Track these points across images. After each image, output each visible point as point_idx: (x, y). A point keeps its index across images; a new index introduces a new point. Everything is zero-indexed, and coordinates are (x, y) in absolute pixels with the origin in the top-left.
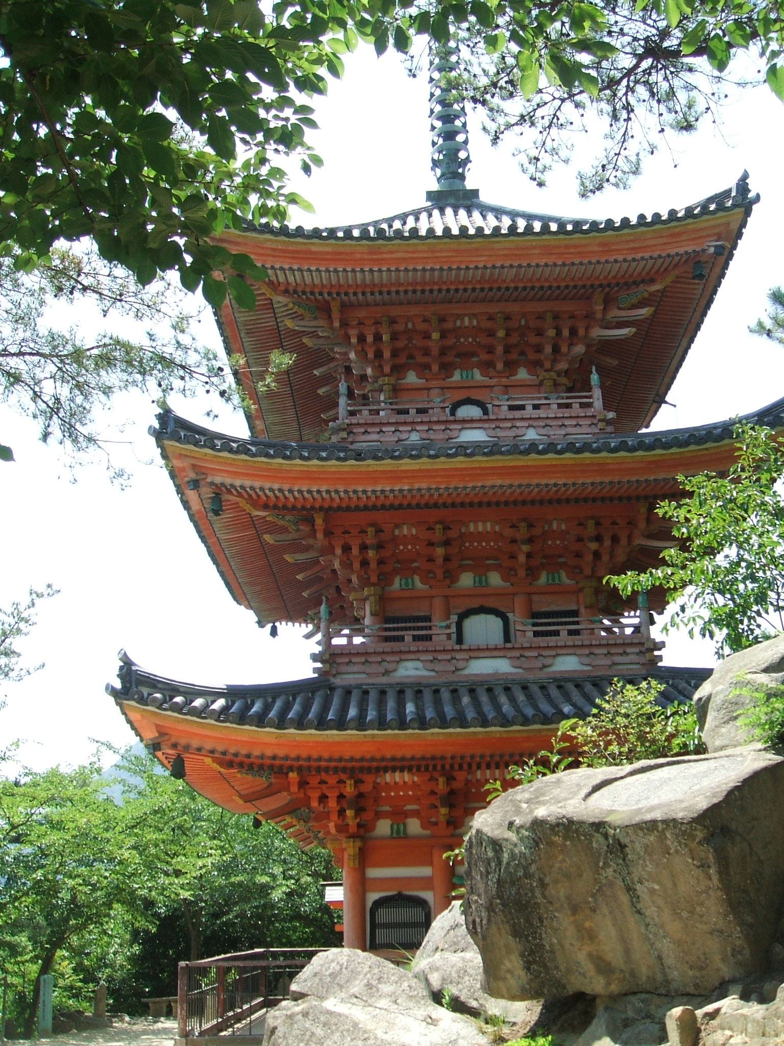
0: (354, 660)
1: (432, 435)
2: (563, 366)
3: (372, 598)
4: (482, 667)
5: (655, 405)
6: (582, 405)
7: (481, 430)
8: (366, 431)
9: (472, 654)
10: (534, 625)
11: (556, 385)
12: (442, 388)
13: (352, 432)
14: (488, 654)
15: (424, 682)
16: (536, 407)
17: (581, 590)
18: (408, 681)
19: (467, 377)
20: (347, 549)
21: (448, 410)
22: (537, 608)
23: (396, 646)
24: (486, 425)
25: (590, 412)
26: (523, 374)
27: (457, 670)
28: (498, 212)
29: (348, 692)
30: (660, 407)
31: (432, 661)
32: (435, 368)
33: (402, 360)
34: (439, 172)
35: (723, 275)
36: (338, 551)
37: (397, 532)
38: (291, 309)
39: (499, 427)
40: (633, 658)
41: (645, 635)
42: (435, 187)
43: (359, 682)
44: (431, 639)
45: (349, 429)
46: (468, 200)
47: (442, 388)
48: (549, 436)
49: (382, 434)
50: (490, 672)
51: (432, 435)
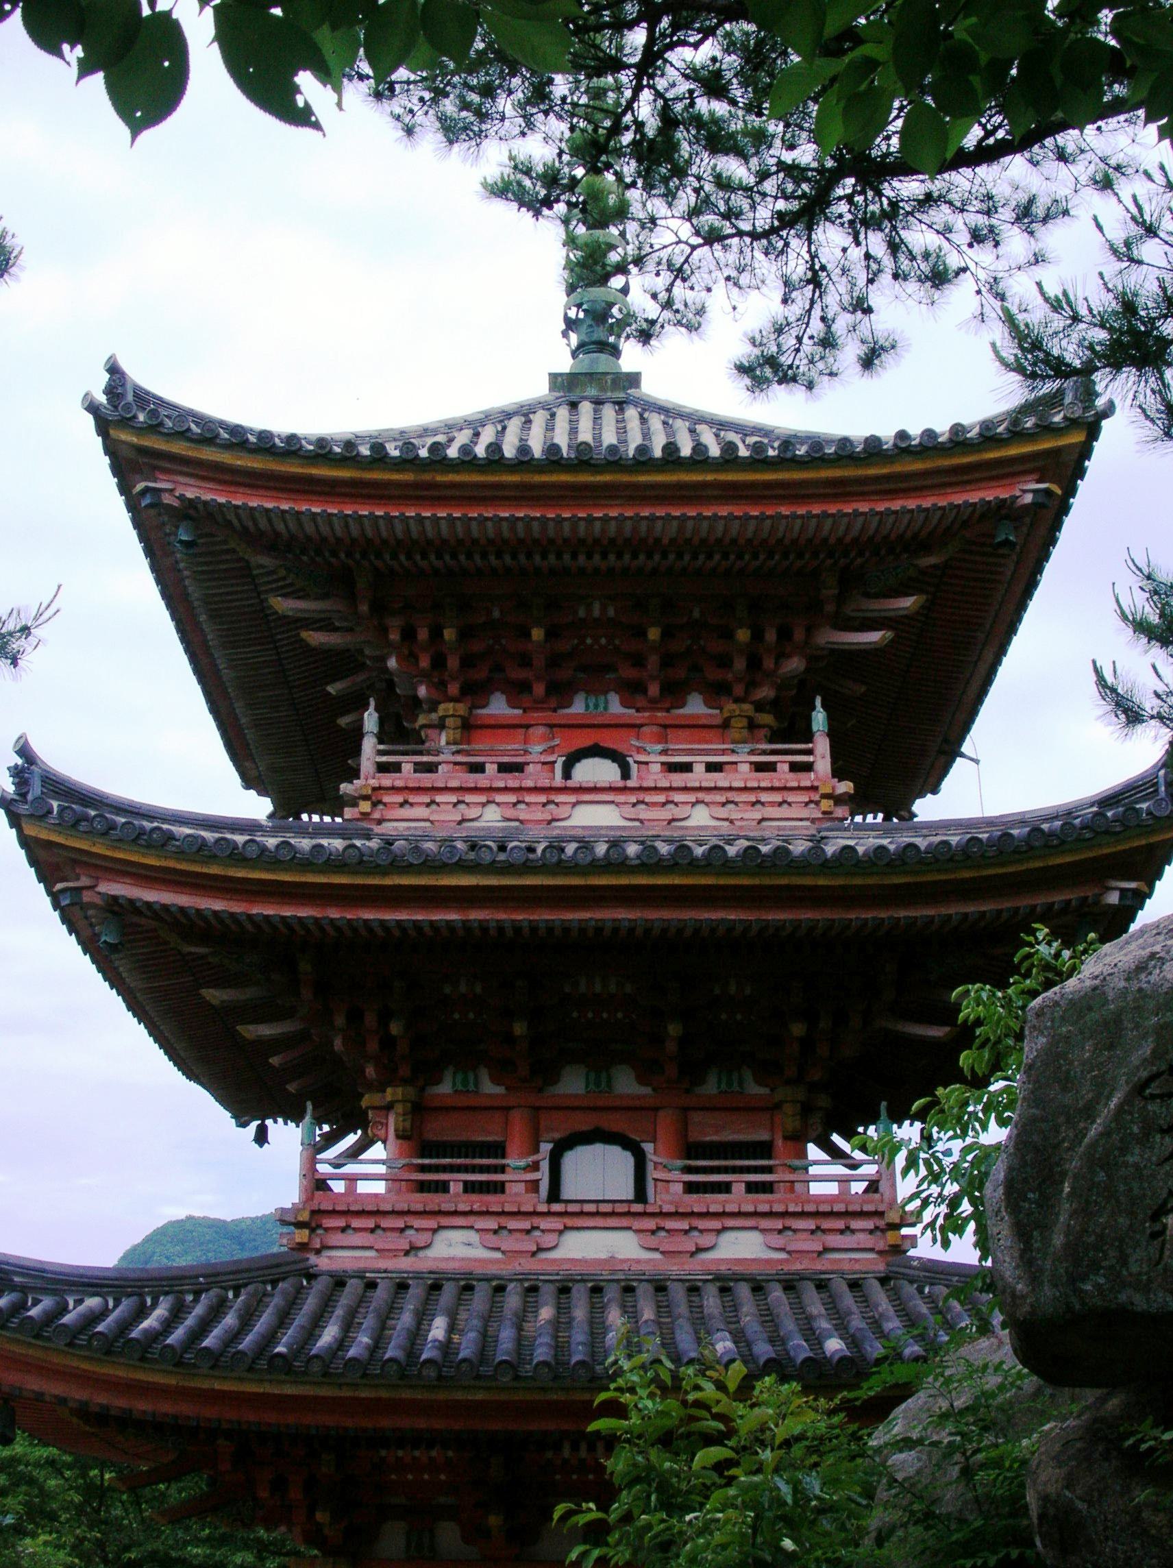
0: (356, 1223)
1: (522, 812)
2: (765, 692)
3: (399, 1108)
4: (586, 1247)
5: (943, 759)
6: (795, 767)
7: (613, 807)
8: (406, 802)
9: (570, 1222)
10: (689, 1170)
11: (752, 726)
12: (551, 726)
13: (380, 802)
14: (599, 1222)
15: (479, 1271)
16: (712, 767)
17: (777, 1107)
18: (451, 1266)
19: (596, 706)
20: (355, 1016)
21: (558, 768)
22: (695, 1136)
23: (434, 1201)
24: (620, 798)
25: (806, 779)
26: (695, 707)
27: (540, 1250)
28: (668, 412)
29: (339, 1282)
30: (953, 761)
31: (495, 1232)
32: (539, 689)
33: (480, 674)
34: (574, 339)
35: (1053, 541)
36: (340, 1021)
37: (447, 990)
38: (284, 578)
39: (643, 802)
40: (863, 1239)
41: (887, 1195)
42: (565, 364)
43: (362, 1265)
44: (503, 1191)
45: (374, 797)
46: (621, 390)
47: (551, 726)
48: (731, 822)
49: (434, 807)
50: (603, 1256)
51: (522, 812)
